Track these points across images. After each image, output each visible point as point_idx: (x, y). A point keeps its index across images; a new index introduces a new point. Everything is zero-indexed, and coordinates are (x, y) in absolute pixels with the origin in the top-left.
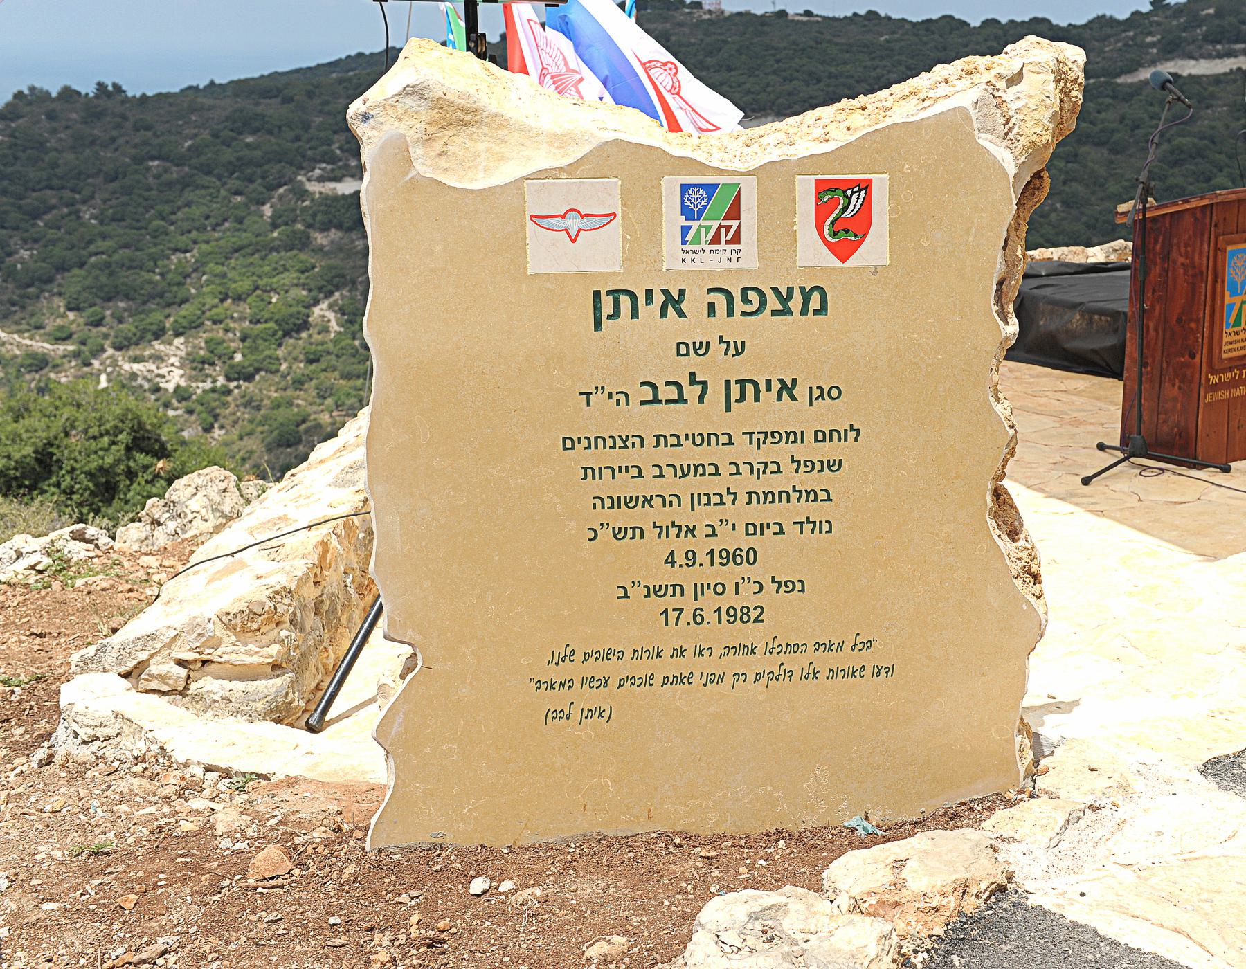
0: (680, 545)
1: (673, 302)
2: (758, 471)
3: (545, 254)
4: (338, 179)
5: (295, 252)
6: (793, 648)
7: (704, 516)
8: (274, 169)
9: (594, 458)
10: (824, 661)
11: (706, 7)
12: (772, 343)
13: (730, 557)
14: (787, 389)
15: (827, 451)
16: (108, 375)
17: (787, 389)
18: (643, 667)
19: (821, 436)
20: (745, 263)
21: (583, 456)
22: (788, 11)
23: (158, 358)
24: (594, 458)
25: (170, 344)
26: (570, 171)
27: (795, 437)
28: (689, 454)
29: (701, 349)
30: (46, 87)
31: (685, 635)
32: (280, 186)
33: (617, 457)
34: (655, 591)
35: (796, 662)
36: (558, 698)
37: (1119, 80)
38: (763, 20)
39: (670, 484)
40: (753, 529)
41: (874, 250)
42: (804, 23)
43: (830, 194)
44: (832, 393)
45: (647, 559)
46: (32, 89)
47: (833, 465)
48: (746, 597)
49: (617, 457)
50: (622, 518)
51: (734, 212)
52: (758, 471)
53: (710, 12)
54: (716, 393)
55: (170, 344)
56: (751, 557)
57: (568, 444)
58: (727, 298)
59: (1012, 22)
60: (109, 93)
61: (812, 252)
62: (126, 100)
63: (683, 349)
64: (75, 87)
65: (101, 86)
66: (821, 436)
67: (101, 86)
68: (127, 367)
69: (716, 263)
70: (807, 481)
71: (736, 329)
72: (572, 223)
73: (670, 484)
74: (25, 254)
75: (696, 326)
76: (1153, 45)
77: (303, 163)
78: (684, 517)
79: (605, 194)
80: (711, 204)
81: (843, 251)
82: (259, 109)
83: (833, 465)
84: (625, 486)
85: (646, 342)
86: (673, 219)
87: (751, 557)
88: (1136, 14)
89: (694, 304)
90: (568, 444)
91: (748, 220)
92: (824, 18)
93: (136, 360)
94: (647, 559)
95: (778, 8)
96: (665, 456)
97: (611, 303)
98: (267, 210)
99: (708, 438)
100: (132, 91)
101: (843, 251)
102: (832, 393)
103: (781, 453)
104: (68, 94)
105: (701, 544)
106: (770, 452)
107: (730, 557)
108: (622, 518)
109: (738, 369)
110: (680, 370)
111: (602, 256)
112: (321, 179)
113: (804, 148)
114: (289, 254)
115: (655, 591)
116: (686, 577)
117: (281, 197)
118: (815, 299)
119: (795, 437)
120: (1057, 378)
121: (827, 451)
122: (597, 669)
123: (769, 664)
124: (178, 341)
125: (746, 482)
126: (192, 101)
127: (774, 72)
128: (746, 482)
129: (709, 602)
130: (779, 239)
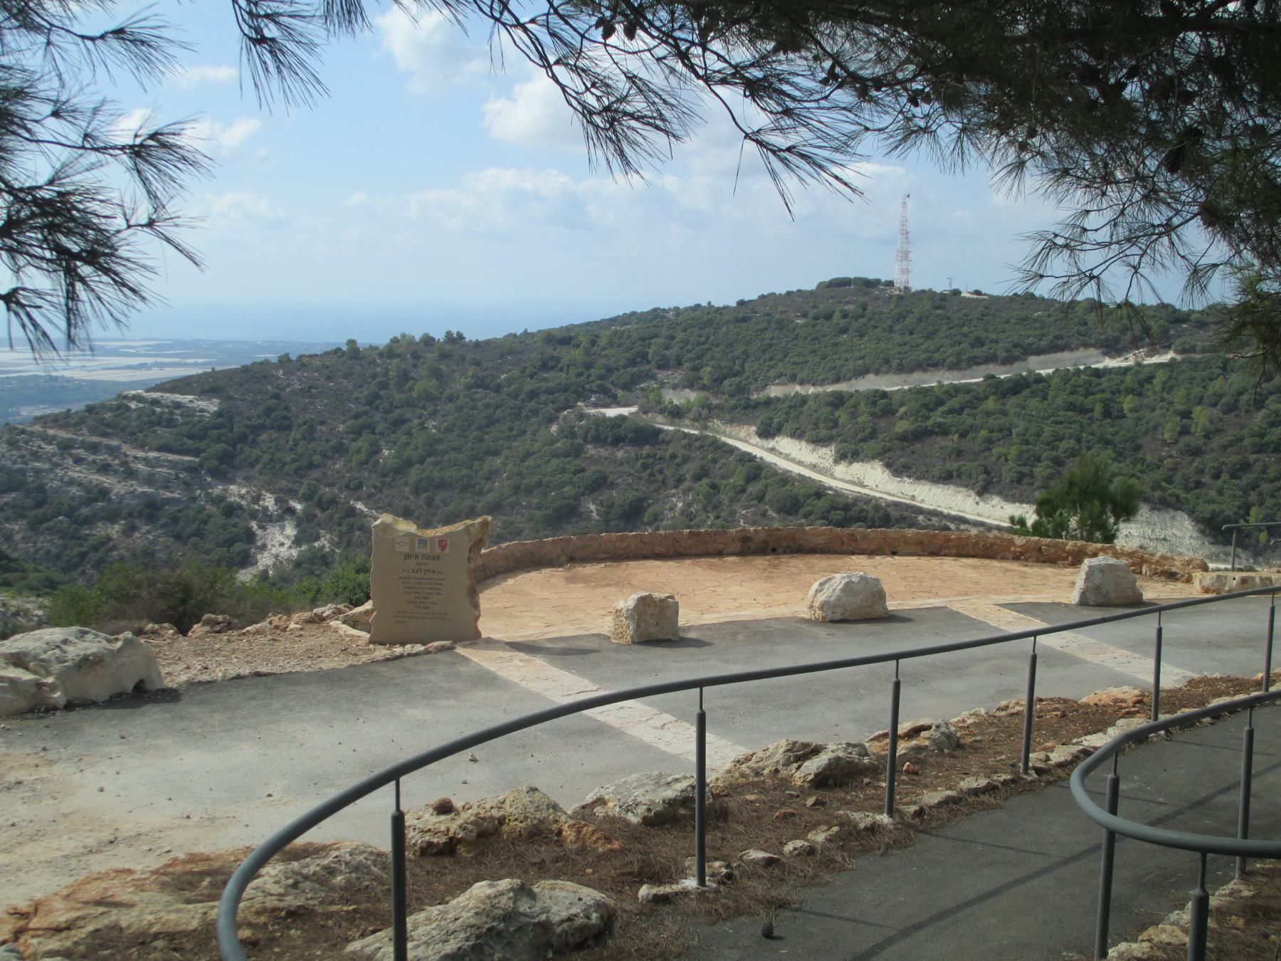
3: (398, 549)
4: (607, 406)
8: (561, 397)
11: (897, 285)
20: (427, 551)
30: (412, 333)
32: (565, 409)
38: (943, 297)
41: (447, 551)
42: (974, 300)
43: (440, 542)
60: (455, 340)
61: (438, 550)
62: (465, 345)
64: (432, 334)
65: (449, 334)
67: (449, 334)
74: (386, 452)
75: (420, 560)
77: (582, 394)
79: (407, 540)
80: (423, 541)
82: (555, 353)
85: (412, 563)
92: (990, 296)
95: (954, 287)
97: (407, 556)
98: (554, 428)
100: (470, 336)
104: (428, 341)
111: (406, 549)
112: (596, 406)
117: (565, 418)
118: (438, 558)
120: (975, 567)
126: (511, 349)
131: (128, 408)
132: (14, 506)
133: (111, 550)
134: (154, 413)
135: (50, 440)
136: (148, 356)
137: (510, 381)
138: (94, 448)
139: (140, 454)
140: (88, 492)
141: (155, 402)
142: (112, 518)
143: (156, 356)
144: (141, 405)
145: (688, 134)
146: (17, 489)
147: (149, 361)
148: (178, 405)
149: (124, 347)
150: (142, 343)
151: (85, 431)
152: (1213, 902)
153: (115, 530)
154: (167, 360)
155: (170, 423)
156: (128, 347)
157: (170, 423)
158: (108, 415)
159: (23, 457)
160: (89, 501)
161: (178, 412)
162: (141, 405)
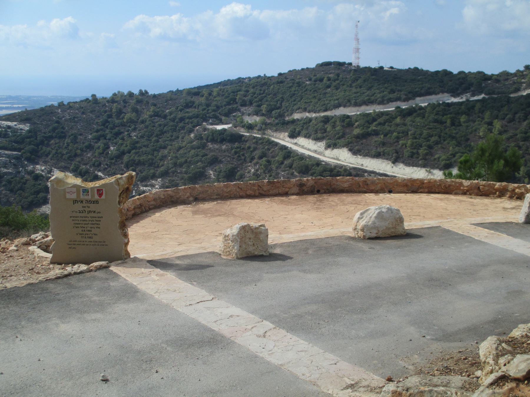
0: (83, 229)
1: (82, 202)
2: (92, 221)
3: (68, 196)
5: (200, 150)
6: (96, 242)
7: (86, 226)
8: (195, 120)
9: (74, 219)
10: (100, 244)
12: (93, 207)
13: (89, 231)
14: (94, 212)
15: (99, 219)
16: (136, 191)
17: (94, 212)
18: (79, 243)
19: (98, 217)
20: (89, 198)
21: (72, 218)
22: (384, 66)
23: (153, 186)
24: (74, 219)
25: (157, 181)
26: (71, 187)
27: (95, 217)
28: (84, 219)
29: (85, 207)
31: (84, 239)
33: (76, 219)
34: (81, 234)
35: (96, 243)
36: (70, 246)
37: (512, 95)
39: (82, 222)
40: (91, 228)
41: (103, 197)
44: (100, 213)
45: (80, 230)
46: (119, 92)
47: (100, 221)
48: (91, 236)
49: (76, 219)
50: (77, 225)
51: (88, 192)
52: (92, 221)
53: (355, 66)
54: (87, 212)
55: (157, 181)
56: (91, 231)
57: (71, 217)
58: (88, 201)
59: (470, 72)
60: (143, 93)
61: (97, 197)
63: (83, 207)
64: (132, 91)
66: (98, 217)
68: (142, 188)
69: (86, 197)
70: (97, 223)
71: (89, 205)
72: (71, 193)
73: (82, 222)
76: (524, 83)
78: (84, 226)
79: (74, 190)
80: (86, 191)
81: (100, 197)
83: (100, 221)
84: (77, 222)
86: (82, 193)
87: (91, 231)
88: (518, 71)
89: (84, 202)
90: (71, 217)
91: (90, 193)
93: (146, 186)
94: (80, 230)
96: (81, 219)
97: (75, 201)
99: (86, 217)
101: (100, 197)
102: (100, 213)
103: (94, 219)
105: (85, 229)
106: (93, 219)
107: (89, 231)
108: (77, 225)
109: (89, 209)
110: (83, 209)
111: (74, 196)
113: (97, 185)
114: (198, 150)
115: (81, 234)
116: (84, 233)
117: (197, 130)
118: (97, 202)
119: (95, 217)
121: (99, 219)
122: (75, 243)
123: (93, 243)
124: (159, 180)
125: (90, 222)
126: (173, 97)
127: (377, 89)
128: (90, 222)
129: (87, 236)
130: (93, 196)
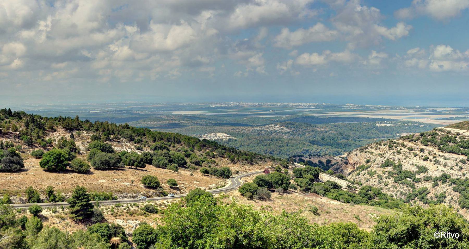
131: (437, 134)
132: (389, 173)
133: (428, 193)
134: (448, 137)
135: (404, 146)
136: (454, 114)
137: (24, 148)
138: (422, 151)
139: (441, 154)
140: (419, 168)
141: (449, 132)
142: (427, 179)
143: (458, 114)
144: (443, 133)
145: (72, 213)
146: (391, 165)
147: (454, 116)
148: (458, 134)
149: (442, 111)
150: (451, 109)
151: (419, 143)
152: (113, 47)
153: (429, 185)
154: (462, 116)
155: (455, 142)
156: (445, 111)
157: (455, 142)
158: (429, 137)
159: (394, 153)
160: (419, 173)
161: (458, 136)
162: (443, 133)
